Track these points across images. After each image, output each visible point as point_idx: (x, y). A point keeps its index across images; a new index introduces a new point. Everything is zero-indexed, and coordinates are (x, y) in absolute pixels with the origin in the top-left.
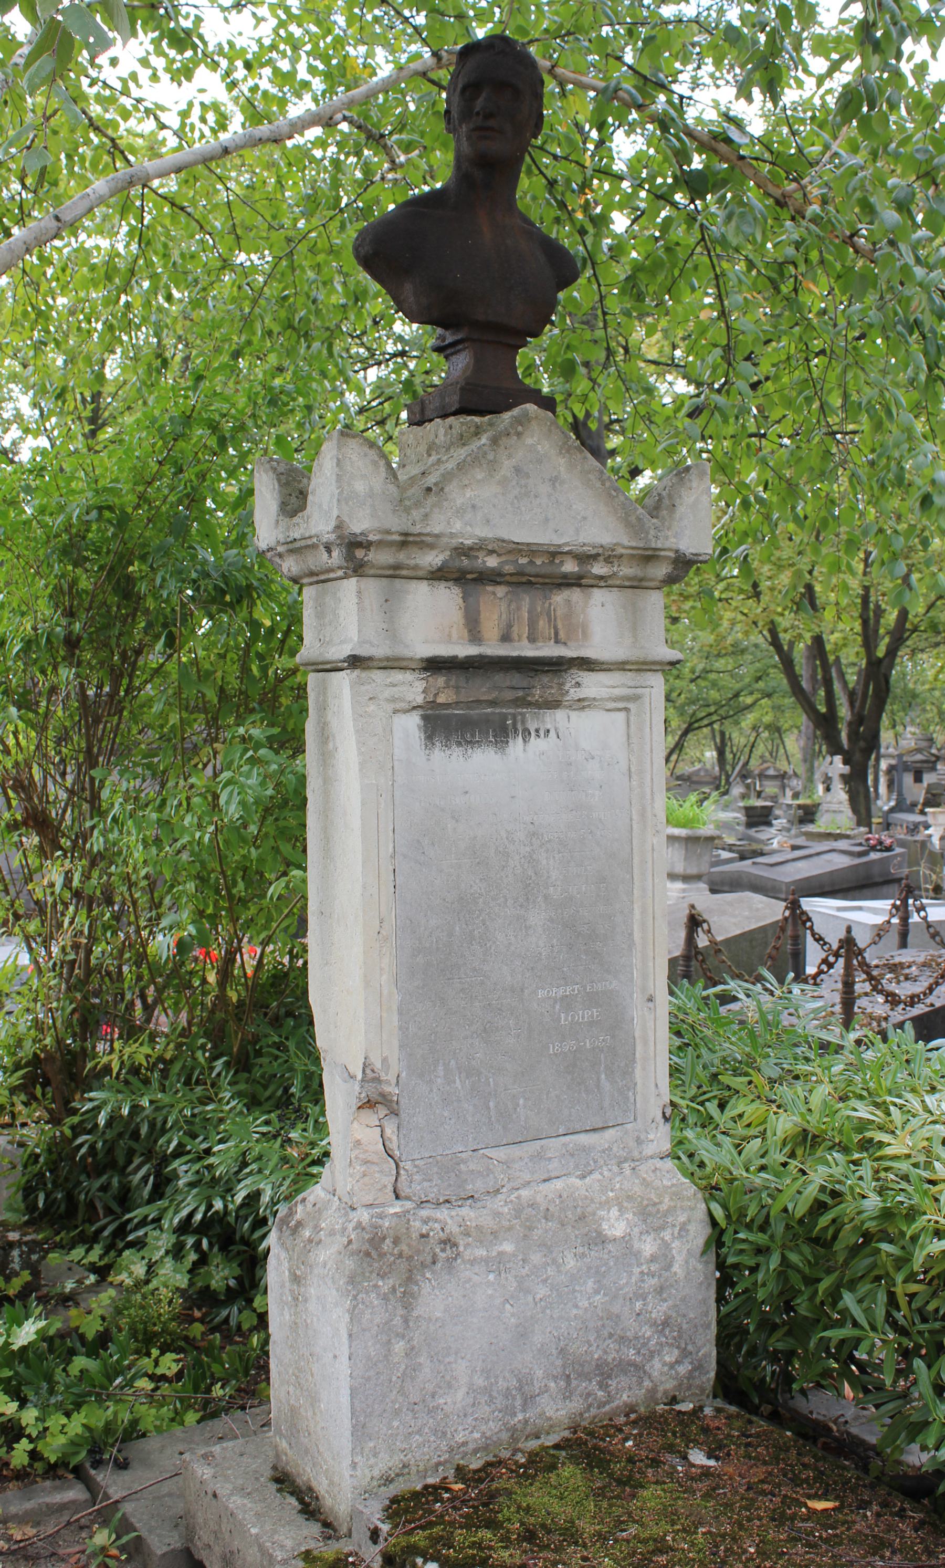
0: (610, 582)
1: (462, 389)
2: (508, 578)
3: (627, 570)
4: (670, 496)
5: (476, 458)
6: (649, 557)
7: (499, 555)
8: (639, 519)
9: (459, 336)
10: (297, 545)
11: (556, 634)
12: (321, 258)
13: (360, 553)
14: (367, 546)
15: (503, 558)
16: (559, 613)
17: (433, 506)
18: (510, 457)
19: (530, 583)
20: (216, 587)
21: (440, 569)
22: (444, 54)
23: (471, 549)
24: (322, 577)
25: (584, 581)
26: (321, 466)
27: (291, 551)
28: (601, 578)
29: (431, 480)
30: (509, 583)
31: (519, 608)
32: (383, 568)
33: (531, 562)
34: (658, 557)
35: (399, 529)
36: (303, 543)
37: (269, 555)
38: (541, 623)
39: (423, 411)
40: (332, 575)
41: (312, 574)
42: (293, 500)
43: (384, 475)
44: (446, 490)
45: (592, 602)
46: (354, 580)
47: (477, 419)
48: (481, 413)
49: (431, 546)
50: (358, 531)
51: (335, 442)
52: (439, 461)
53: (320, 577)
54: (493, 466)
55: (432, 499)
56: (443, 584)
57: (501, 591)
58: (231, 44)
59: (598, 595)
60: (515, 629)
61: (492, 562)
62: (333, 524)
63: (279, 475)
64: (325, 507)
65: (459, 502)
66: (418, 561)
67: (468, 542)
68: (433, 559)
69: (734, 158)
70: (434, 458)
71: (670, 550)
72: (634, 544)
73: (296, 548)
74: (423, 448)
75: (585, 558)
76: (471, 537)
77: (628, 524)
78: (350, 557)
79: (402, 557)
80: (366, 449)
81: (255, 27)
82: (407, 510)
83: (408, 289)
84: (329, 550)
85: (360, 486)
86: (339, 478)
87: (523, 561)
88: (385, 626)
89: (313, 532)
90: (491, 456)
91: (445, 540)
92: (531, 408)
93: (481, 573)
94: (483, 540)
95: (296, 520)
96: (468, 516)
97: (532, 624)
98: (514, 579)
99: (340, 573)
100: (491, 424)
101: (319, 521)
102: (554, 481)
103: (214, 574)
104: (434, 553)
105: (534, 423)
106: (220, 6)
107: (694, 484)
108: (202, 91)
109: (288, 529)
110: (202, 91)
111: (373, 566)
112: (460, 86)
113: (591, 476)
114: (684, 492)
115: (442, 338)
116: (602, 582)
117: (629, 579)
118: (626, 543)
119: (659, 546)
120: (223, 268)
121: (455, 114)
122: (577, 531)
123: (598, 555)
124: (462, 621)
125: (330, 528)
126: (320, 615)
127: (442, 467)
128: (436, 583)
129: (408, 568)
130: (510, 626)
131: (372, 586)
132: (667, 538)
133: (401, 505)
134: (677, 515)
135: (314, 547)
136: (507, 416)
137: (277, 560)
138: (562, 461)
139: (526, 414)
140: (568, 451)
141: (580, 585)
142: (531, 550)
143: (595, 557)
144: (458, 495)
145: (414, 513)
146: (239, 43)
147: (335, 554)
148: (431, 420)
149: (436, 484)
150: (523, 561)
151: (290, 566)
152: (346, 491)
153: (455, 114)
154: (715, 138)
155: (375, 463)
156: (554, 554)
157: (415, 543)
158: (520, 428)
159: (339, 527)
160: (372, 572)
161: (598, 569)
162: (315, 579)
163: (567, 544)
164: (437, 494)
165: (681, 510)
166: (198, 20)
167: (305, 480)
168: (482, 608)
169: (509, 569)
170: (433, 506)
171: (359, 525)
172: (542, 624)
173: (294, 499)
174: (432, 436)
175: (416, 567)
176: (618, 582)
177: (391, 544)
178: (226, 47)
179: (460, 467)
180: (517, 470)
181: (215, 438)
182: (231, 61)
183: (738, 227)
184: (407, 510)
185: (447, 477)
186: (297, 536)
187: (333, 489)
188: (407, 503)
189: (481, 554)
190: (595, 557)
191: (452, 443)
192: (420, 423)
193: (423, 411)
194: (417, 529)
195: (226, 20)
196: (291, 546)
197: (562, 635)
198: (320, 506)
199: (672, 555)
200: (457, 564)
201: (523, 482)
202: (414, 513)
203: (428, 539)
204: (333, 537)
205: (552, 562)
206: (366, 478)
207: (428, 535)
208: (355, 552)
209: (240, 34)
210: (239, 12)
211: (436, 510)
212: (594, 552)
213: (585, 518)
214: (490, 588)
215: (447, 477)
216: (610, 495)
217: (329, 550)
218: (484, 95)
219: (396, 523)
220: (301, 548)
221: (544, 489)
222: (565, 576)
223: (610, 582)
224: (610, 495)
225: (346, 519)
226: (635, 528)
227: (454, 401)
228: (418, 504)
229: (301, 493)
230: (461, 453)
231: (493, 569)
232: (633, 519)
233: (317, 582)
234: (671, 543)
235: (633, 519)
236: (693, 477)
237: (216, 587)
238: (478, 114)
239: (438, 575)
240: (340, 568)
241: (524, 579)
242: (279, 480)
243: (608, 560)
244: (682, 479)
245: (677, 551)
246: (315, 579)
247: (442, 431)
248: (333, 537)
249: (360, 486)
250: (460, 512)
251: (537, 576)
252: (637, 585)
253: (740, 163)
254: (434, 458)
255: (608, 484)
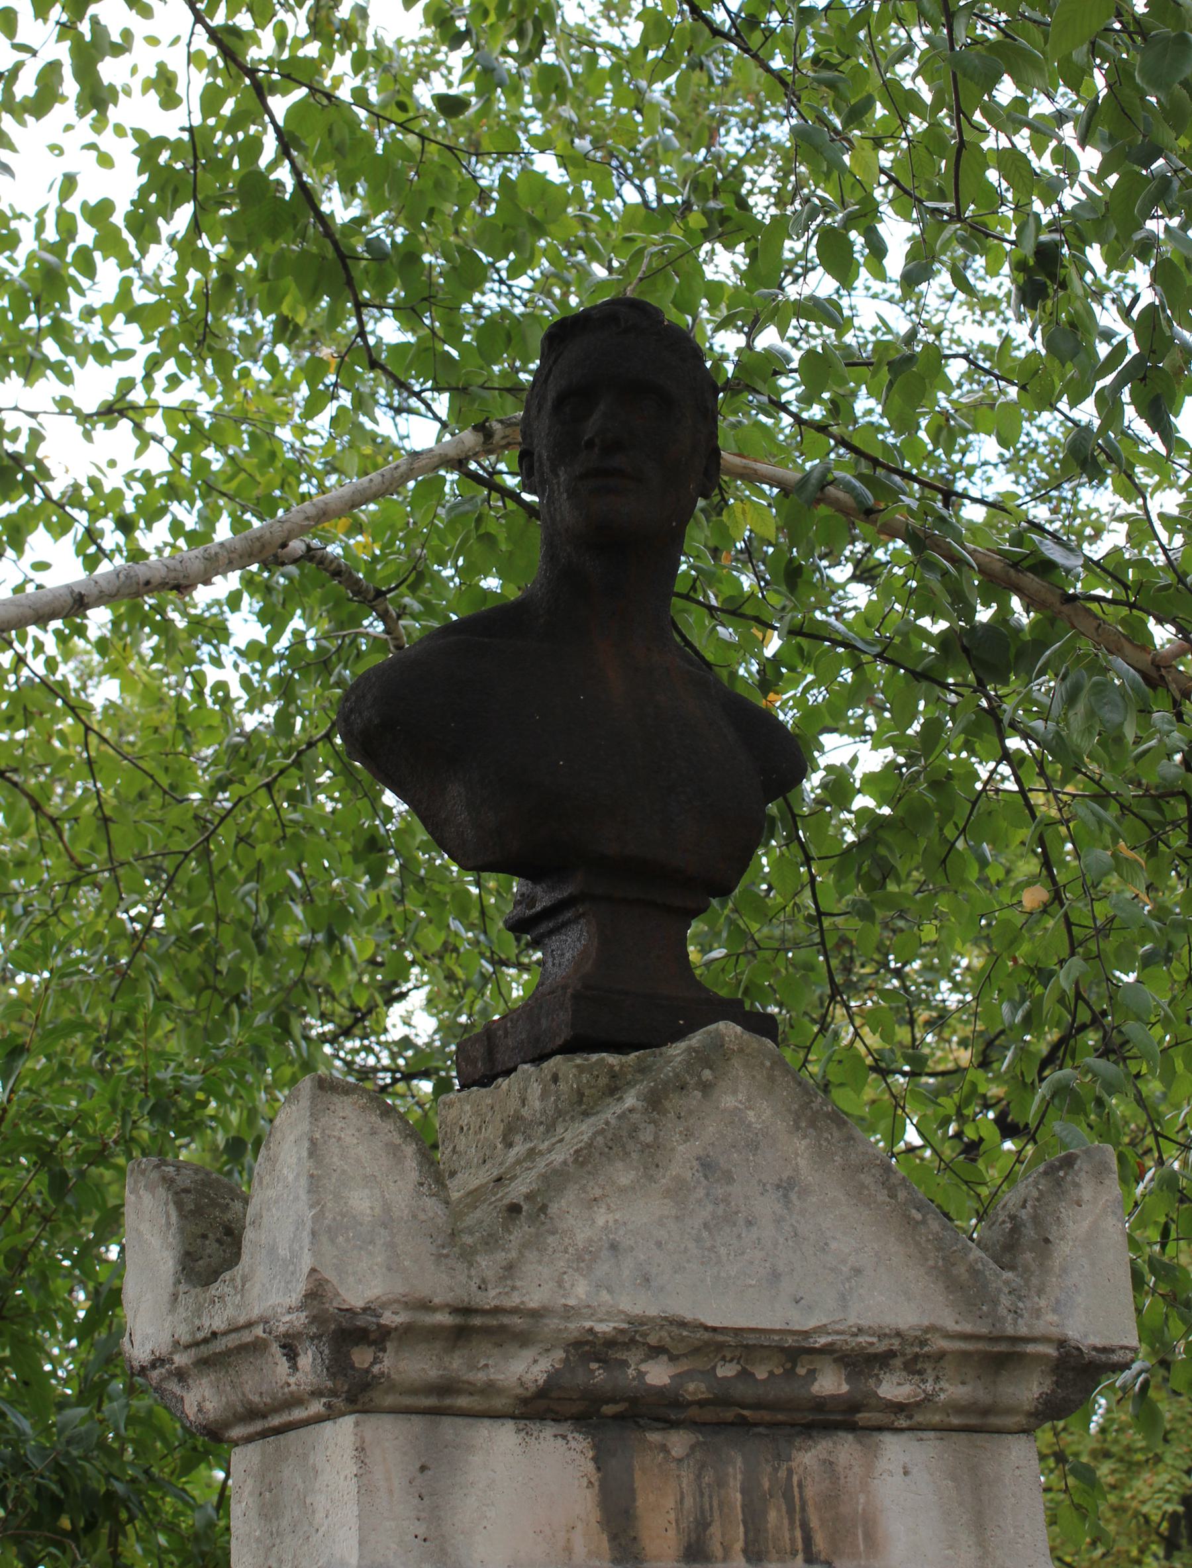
0: (919, 1418)
1: (576, 997)
2: (693, 1412)
3: (954, 1390)
4: (1036, 1220)
5: (616, 1138)
6: (1000, 1357)
7: (673, 1358)
8: (974, 1273)
9: (558, 895)
10: (220, 1346)
11: (808, 1540)
12: (262, 850)
13: (362, 1357)
14: (378, 1337)
15: (684, 1366)
16: (810, 1492)
17: (525, 1245)
18: (688, 1135)
19: (743, 1423)
20: (40, 1491)
21: (542, 1393)
22: (497, 426)
23: (611, 1343)
24: (276, 1421)
25: (862, 1417)
26: (273, 1161)
27: (205, 1363)
28: (900, 1408)
29: (518, 1190)
30: (695, 1425)
31: (721, 1483)
32: (414, 1391)
33: (745, 1374)
34: (1021, 1356)
35: (449, 1297)
36: (232, 1341)
37: (155, 1374)
38: (772, 1516)
39: (491, 1052)
40: (298, 1414)
41: (252, 1413)
42: (211, 1246)
43: (414, 1176)
44: (553, 1209)
45: (882, 1464)
46: (347, 1423)
47: (612, 1059)
48: (620, 1048)
49: (523, 1339)
50: (358, 1303)
51: (305, 1102)
52: (532, 1154)
53: (269, 1421)
54: (653, 1156)
55: (521, 1232)
56: (549, 1430)
57: (679, 1442)
58: (94, 483)
59: (896, 1451)
60: (715, 1530)
61: (658, 1374)
62: (300, 1287)
63: (179, 1196)
64: (283, 1252)
65: (581, 1237)
66: (494, 1375)
67: (603, 1328)
68: (526, 1369)
69: (1055, 600)
70: (519, 1149)
71: (1045, 1339)
72: (968, 1328)
73: (215, 1355)
74: (493, 1132)
75: (862, 1362)
76: (609, 1316)
77: (952, 1285)
78: (338, 1365)
79: (456, 1364)
80: (374, 1119)
81: (139, 453)
82: (468, 1256)
83: (456, 793)
84: (291, 1354)
85: (361, 1202)
86: (315, 1183)
87: (726, 1371)
88: (421, 1530)
89: (255, 1313)
90: (647, 1136)
91: (553, 1323)
92: (728, 1029)
93: (634, 1401)
94: (637, 1322)
95: (216, 1289)
96: (603, 1268)
97: (753, 1519)
98: (708, 1415)
99: (316, 1407)
100: (643, 1070)
101: (268, 1289)
102: (786, 1188)
103: (38, 1464)
104: (528, 1354)
105: (736, 1062)
106: (77, 412)
107: (1087, 1193)
108: (41, 566)
109: (198, 1313)
110: (41, 566)
111: (392, 1387)
112: (551, 395)
113: (866, 1178)
114: (1066, 1212)
115: (525, 900)
116: (902, 1418)
117: (960, 1410)
118: (950, 1325)
119: (1023, 1331)
120: (76, 882)
121: (543, 452)
122: (843, 1299)
123: (891, 1354)
124: (595, 1515)
125: (295, 1299)
126: (269, 1511)
127: (541, 1165)
128: (534, 1426)
129: (471, 1390)
130: (702, 1525)
131: (390, 1436)
132: (1037, 1313)
133: (454, 1243)
134: (1056, 1263)
135: (257, 1347)
136: (677, 1051)
137: (174, 1386)
138: (801, 1145)
139: (718, 1044)
140: (812, 1124)
141: (852, 1427)
142: (744, 1345)
143: (883, 1360)
144: (580, 1221)
145: (483, 1261)
146: (112, 481)
147: (305, 1360)
148: (507, 1073)
149: (529, 1197)
150: (726, 1371)
151: (202, 1399)
152: (327, 1215)
153: (543, 452)
154: (1015, 565)
155: (394, 1150)
156: (796, 1352)
157: (486, 1331)
158: (707, 1074)
159: (315, 1294)
160: (389, 1400)
161: (893, 1388)
162: (258, 1426)
163: (821, 1330)
164: (533, 1219)
165: (1063, 1250)
166: (36, 437)
167: (237, 1205)
168: (639, 1481)
169: (695, 1389)
170: (525, 1245)
171: (363, 1287)
172: (774, 1516)
173: (212, 1241)
174: (513, 1104)
175: (489, 1389)
176: (936, 1419)
177: (433, 1333)
178: (87, 492)
179: (583, 1158)
180: (707, 1166)
181: (44, 1177)
182: (95, 515)
183: (1091, 714)
184: (468, 1256)
185: (555, 1181)
186: (219, 1324)
187: (302, 1208)
188: (468, 1240)
189: (633, 1357)
190: (883, 1360)
191: (560, 1113)
192: (486, 1081)
193: (491, 1052)
194: (491, 1298)
195: (88, 435)
196: (205, 1351)
197: (820, 1542)
198: (272, 1250)
199: (1050, 1350)
200: (580, 1379)
201: (720, 1191)
202: (483, 1261)
203: (516, 1321)
204: (299, 1319)
205: (790, 1373)
206: (376, 1182)
207: (515, 1311)
208: (351, 1355)
209: (112, 463)
210: (110, 425)
211: (532, 1255)
212: (882, 1347)
213: (857, 1271)
214: (654, 1437)
215: (555, 1181)
216: (908, 1218)
217: (291, 1354)
218: (602, 407)
219: (443, 1285)
220: (228, 1353)
221: (766, 1206)
222: (820, 1404)
223: (919, 1418)
224: (908, 1218)
225: (329, 1274)
226: (968, 1291)
227: (561, 1025)
228: (491, 1242)
229: (229, 1231)
230: (582, 1131)
231: (660, 1391)
232: (961, 1271)
233: (264, 1434)
234: (1049, 1323)
235: (961, 1271)
236: (1082, 1178)
237: (40, 1491)
238: (590, 444)
239: (537, 1408)
240: (316, 1394)
241: (730, 1415)
242: (179, 1205)
243: (913, 1367)
244: (1059, 1183)
245: (1062, 1343)
246: (258, 1426)
247: (535, 1089)
248: (299, 1319)
249: (361, 1202)
250: (584, 1259)
251: (758, 1406)
252: (978, 1423)
253: (1066, 609)
254: (519, 1149)
255: (902, 1195)
